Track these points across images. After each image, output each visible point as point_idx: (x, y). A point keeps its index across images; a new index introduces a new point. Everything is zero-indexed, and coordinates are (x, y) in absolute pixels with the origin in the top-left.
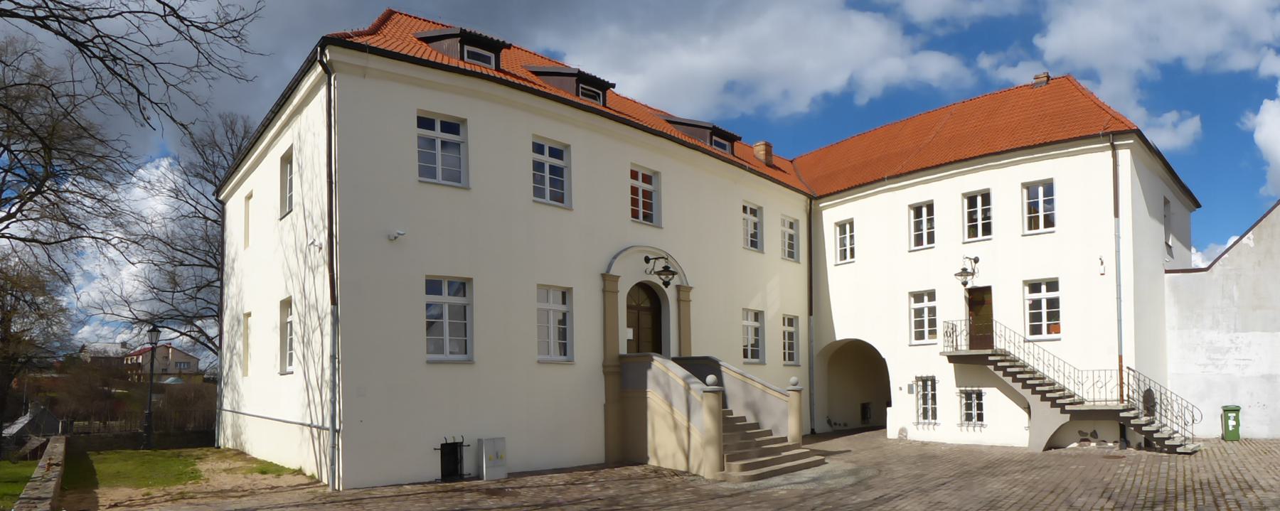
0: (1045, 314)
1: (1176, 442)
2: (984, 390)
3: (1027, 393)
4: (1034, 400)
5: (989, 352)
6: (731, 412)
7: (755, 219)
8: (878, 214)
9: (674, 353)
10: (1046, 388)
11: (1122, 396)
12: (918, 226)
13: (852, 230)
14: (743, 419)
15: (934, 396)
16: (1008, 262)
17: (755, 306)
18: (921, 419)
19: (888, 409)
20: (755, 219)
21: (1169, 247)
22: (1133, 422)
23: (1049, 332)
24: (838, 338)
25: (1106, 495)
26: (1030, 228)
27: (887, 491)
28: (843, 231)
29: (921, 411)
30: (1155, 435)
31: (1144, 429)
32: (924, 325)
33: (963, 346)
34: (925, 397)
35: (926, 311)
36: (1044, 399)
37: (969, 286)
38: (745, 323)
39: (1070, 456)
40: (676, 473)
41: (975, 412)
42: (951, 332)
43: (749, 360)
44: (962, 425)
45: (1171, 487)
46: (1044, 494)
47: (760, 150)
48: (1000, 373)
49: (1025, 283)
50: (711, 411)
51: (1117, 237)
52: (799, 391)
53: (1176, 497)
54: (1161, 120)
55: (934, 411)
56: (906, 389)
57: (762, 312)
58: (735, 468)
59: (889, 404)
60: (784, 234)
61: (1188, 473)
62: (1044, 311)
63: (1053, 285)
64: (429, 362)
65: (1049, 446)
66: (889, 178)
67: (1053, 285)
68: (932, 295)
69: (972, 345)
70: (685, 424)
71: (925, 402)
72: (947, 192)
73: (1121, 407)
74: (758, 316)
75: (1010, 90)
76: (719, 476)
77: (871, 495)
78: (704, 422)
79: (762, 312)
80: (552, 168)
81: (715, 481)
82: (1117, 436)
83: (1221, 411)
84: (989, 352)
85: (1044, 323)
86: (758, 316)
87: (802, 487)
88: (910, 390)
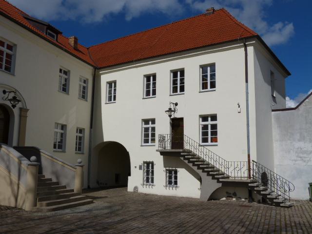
0: (210, 133)
1: (280, 201)
2: (178, 169)
3: (200, 172)
4: (204, 175)
5: (181, 150)
6: (44, 176)
7: (66, 77)
8: (128, 79)
9: (15, 144)
10: (210, 170)
11: (250, 175)
12: (148, 86)
13: (115, 86)
14: (50, 180)
15: (153, 172)
16: (192, 105)
17: (62, 121)
18: (145, 183)
19: (129, 177)
20: (66, 77)
21: (274, 98)
22: (255, 189)
23: (212, 142)
24: (105, 140)
25: (242, 224)
26: (203, 89)
27: (124, 217)
28: (110, 87)
29: (145, 179)
30: (268, 196)
31: (262, 192)
32: (148, 136)
33: (168, 147)
34: (148, 172)
35: (150, 129)
36: (208, 175)
37: (172, 117)
38: (56, 130)
39: (221, 204)
40: (8, 208)
41: (173, 180)
42: (162, 139)
43: (57, 149)
44: (166, 186)
45: (278, 224)
46: (207, 221)
47: (72, 41)
48: (186, 161)
49: (201, 116)
50: (32, 173)
51: (247, 93)
52: (82, 166)
53: (281, 230)
54: (272, 28)
55: (153, 179)
56: (138, 167)
57: (66, 125)
58: (43, 206)
59: (130, 175)
60: (80, 85)
61: (287, 217)
62: (209, 130)
63: (214, 117)
64: (54, 151)
65: (211, 198)
66: (136, 61)
67: (214, 117)
68: (153, 121)
69: (173, 147)
70: (17, 182)
71: (148, 174)
72: (163, 69)
73: (249, 181)
74: (63, 127)
75: (199, 14)
76: (35, 209)
77: (117, 219)
78: (28, 180)
79: (66, 125)
80: (7, 54)
81: (31, 212)
82: (247, 196)
83: (309, 186)
84: (181, 150)
85: (209, 136)
86: (63, 127)
87: (80, 215)
88: (140, 168)
